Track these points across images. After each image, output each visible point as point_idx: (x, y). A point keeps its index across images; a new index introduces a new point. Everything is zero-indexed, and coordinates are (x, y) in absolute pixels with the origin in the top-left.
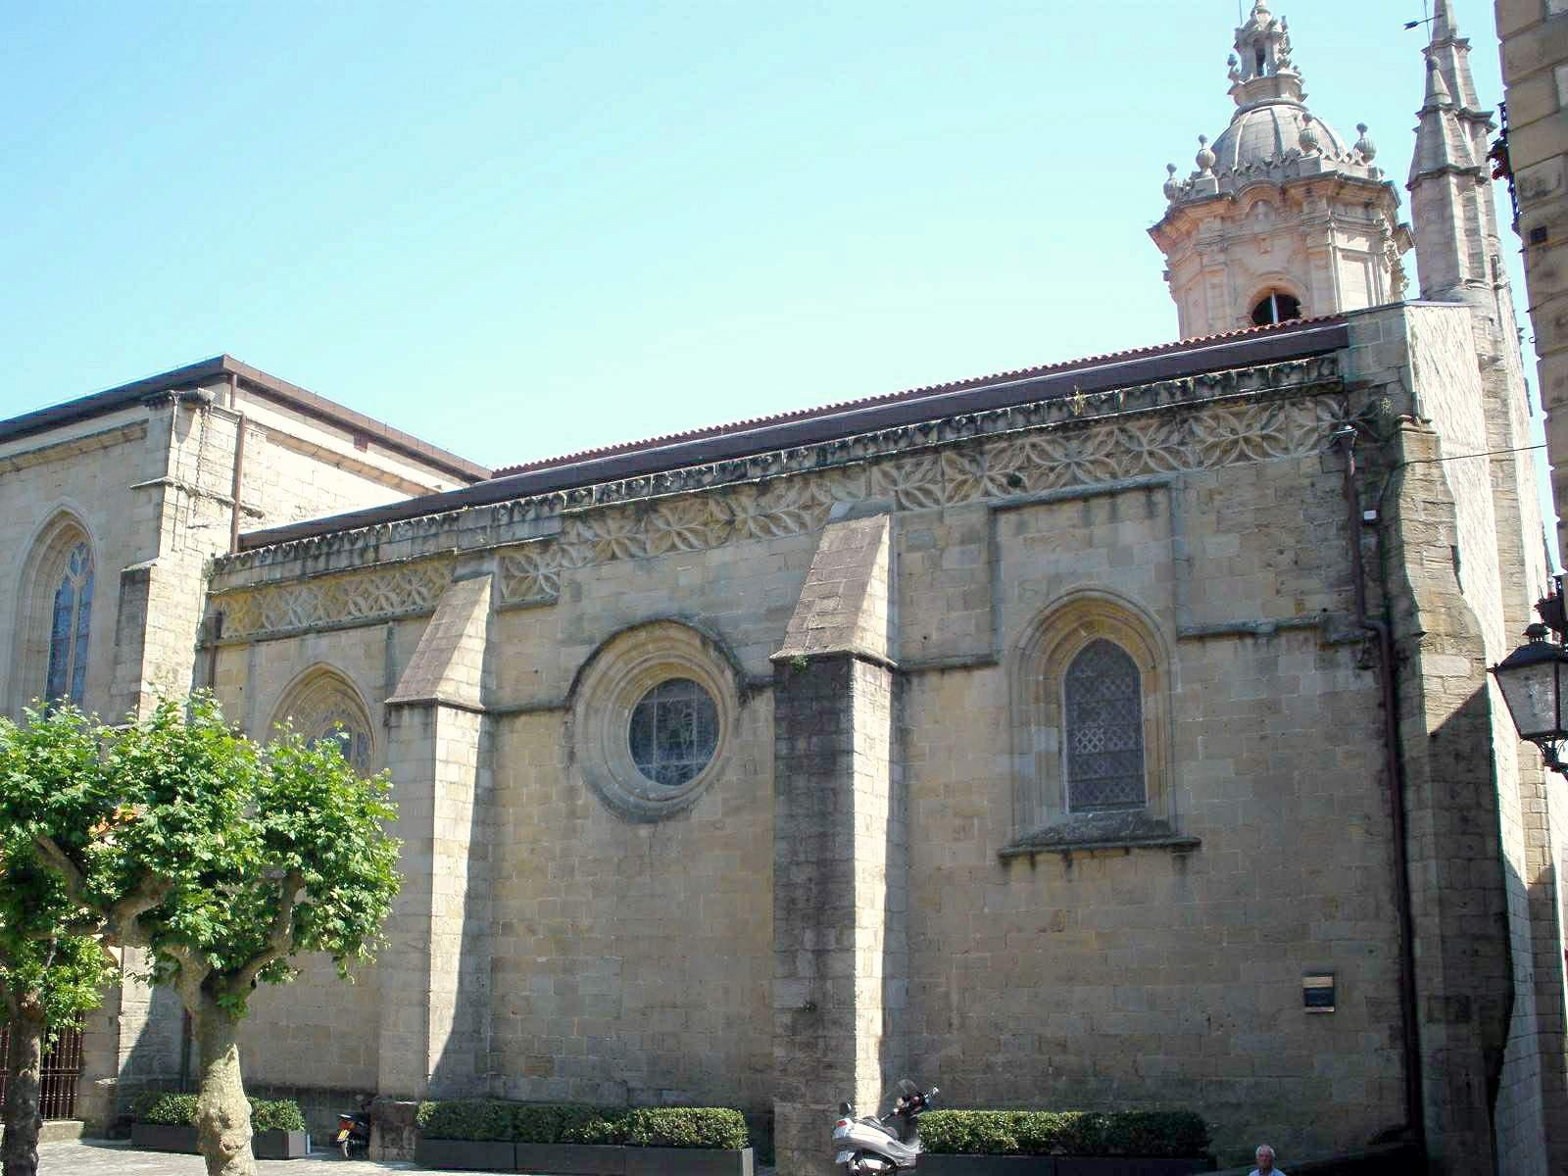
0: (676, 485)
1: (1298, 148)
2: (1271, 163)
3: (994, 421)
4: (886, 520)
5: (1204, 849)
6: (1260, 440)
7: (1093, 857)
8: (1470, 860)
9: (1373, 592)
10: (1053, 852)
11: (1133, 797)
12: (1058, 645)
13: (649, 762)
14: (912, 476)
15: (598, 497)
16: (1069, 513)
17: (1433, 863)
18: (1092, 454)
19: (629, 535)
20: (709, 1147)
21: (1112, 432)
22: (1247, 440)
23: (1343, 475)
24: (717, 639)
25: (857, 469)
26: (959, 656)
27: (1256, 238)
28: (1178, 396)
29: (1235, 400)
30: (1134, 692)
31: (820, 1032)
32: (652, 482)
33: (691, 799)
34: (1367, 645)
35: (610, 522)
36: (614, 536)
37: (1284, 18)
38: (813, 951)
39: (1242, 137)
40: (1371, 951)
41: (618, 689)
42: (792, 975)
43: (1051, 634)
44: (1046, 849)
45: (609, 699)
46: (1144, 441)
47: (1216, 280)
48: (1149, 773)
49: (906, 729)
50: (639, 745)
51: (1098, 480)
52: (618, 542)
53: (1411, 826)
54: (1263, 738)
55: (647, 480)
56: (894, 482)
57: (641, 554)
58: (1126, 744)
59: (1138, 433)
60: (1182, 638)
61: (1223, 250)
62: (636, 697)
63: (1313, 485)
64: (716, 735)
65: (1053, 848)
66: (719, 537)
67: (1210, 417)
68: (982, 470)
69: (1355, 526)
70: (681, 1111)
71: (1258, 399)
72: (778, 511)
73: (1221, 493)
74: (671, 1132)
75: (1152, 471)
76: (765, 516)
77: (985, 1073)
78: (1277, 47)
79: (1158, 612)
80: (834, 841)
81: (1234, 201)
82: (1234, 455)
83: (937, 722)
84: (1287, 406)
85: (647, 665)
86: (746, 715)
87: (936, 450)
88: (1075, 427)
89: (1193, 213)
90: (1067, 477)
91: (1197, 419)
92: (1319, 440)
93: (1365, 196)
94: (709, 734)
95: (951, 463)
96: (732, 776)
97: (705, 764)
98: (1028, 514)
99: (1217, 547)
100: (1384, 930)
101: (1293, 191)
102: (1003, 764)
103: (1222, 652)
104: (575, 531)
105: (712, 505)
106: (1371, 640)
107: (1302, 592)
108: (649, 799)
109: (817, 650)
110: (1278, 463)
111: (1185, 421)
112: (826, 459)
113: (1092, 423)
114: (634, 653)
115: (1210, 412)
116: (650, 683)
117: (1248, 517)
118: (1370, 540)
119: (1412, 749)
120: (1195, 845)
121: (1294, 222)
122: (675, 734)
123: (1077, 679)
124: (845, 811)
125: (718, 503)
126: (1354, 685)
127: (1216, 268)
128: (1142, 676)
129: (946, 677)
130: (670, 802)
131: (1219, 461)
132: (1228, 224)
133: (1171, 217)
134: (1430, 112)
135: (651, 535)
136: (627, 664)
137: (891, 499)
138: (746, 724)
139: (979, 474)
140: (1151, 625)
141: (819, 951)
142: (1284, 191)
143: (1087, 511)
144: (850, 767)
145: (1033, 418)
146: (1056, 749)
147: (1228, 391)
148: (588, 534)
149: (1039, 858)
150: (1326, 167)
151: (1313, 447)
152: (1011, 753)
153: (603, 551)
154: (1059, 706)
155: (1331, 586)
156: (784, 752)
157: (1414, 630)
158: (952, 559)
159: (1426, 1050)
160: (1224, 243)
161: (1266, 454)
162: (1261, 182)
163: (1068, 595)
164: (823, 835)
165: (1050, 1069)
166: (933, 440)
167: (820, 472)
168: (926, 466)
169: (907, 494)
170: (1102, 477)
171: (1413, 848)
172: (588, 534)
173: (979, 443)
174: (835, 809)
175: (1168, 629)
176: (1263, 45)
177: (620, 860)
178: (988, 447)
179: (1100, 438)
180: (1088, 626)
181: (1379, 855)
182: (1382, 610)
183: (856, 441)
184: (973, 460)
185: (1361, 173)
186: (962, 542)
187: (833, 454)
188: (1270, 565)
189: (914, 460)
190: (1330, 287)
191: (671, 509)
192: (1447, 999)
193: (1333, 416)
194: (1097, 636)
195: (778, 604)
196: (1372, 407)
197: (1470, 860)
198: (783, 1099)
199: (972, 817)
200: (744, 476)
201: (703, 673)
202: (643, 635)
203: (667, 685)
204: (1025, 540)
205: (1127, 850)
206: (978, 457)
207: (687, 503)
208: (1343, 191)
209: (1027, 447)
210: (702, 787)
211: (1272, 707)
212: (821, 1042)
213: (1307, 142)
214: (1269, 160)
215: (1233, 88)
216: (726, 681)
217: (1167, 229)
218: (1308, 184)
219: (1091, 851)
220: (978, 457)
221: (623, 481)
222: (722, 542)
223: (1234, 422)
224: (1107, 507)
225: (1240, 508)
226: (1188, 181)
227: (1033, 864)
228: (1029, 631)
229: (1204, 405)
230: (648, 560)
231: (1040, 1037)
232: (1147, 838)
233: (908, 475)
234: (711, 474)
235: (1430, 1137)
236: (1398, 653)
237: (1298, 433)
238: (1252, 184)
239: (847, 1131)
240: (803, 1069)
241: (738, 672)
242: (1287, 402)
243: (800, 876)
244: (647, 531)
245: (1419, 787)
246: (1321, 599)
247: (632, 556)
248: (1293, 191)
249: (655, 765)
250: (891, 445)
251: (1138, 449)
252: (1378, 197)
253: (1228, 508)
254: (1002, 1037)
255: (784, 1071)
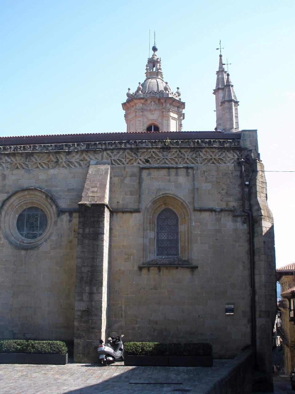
0: (40, 149)
1: (163, 90)
2: (156, 92)
3: (142, 143)
4: (109, 167)
5: (199, 269)
6: (218, 159)
7: (167, 269)
8: (271, 275)
9: (247, 204)
10: (156, 267)
11: (175, 253)
12: (157, 208)
13: (23, 231)
14: (116, 156)
15: (13, 149)
16: (164, 172)
17: (263, 276)
18: (170, 157)
19: (23, 162)
20: (55, 353)
21: (177, 151)
22: (215, 159)
23: (240, 171)
24: (51, 196)
25: (99, 152)
26: (128, 209)
27: (150, 110)
28: (196, 144)
29: (212, 148)
30: (176, 223)
31: (90, 318)
32: (32, 147)
33: (39, 244)
34: (245, 217)
35: (17, 158)
36: (18, 162)
37: (160, 58)
38: (88, 293)
39: (149, 85)
40: (244, 298)
41: (16, 208)
42: (82, 300)
43: (155, 205)
44: (153, 266)
45: (12, 211)
46: (186, 155)
47: (139, 119)
48: (181, 247)
49: (112, 228)
50: (20, 225)
51: (172, 164)
52: (19, 164)
53: (256, 265)
54: (217, 239)
55: (30, 147)
56: (111, 157)
57: (26, 168)
58: (173, 238)
59: (184, 153)
60: (195, 210)
61: (142, 112)
62: (20, 212)
63: (232, 173)
64: (46, 225)
65: (155, 266)
66: (53, 166)
67: (205, 151)
68: (138, 157)
69: (242, 185)
70: (44, 342)
71: (218, 148)
72: (73, 160)
73: (207, 172)
74: (42, 349)
75: (187, 163)
76: (68, 161)
77: (132, 330)
78: (158, 65)
79: (188, 202)
80: (97, 260)
81: (146, 100)
82: (211, 162)
83: (121, 227)
84: (226, 152)
85: (26, 202)
86: (59, 220)
87: (124, 149)
88: (166, 148)
89: (136, 101)
90: (163, 162)
91: (201, 151)
92: (233, 162)
93: (178, 105)
94: (44, 224)
95: (128, 153)
96: (54, 238)
97: (42, 234)
98: (151, 171)
99: (205, 186)
100: (247, 293)
101: (162, 100)
102: (140, 241)
103: (206, 215)
104: (5, 159)
105: (51, 156)
106: (247, 216)
107: (228, 201)
108: (24, 243)
109: (93, 202)
110: (223, 166)
111: (197, 151)
112: (89, 147)
113: (172, 148)
114: (22, 198)
115: (205, 150)
116: (25, 207)
117: (214, 179)
118: (247, 190)
119: (257, 245)
120: (197, 267)
121: (161, 108)
122: (32, 223)
123: (160, 218)
124: (100, 251)
125: (53, 156)
126: (241, 227)
127: (140, 116)
128: (179, 220)
129: (124, 214)
130: (31, 244)
131: (206, 163)
132: (144, 105)
133: (128, 101)
134: (228, 86)
135: (30, 163)
136: (19, 201)
137: (110, 160)
138: (59, 223)
139: (137, 158)
140: (186, 206)
141: (91, 293)
142: (159, 100)
143: (169, 172)
144: (103, 238)
145: (154, 144)
146: (154, 238)
147: (210, 145)
148: (9, 160)
149: (151, 268)
150: (170, 96)
151: (232, 163)
152: (144, 238)
153: (14, 166)
154: (155, 225)
155: (236, 200)
156: (81, 232)
157: (260, 215)
158: (127, 181)
159: (258, 324)
160: (143, 110)
161: (220, 163)
162: (154, 97)
163: (162, 195)
164: (93, 258)
165: (152, 329)
166: (123, 146)
167: (87, 151)
168: (121, 153)
169: (114, 160)
170: (173, 163)
171: (256, 271)
172: (9, 160)
173: (138, 149)
174: (97, 250)
175: (191, 207)
176: (155, 64)
177: (14, 261)
178: (140, 150)
179: (172, 153)
180: (165, 204)
181: (247, 273)
182: (249, 208)
183: (99, 143)
184: (135, 154)
185: (177, 99)
186: (131, 176)
187: (91, 146)
188: (219, 193)
189: (117, 151)
190: (168, 125)
191: (37, 156)
192: (266, 311)
193: (238, 156)
194: (167, 207)
195: (71, 188)
196: (248, 155)
197: (271, 275)
198: (77, 338)
199: (131, 255)
200: (62, 149)
201: (44, 206)
202: (26, 192)
203: (30, 209)
204: (150, 178)
205: (177, 268)
206: (137, 153)
207: (43, 155)
208: (174, 103)
209: (152, 152)
210: (43, 240)
211: (219, 231)
212: (90, 321)
213: (166, 89)
214: (155, 91)
215: (146, 72)
216: (53, 209)
217: (127, 104)
218: (166, 99)
219: (167, 267)
220: (137, 153)
221: (22, 146)
222: (54, 168)
223: (211, 153)
224: (175, 171)
225: (212, 177)
226: (134, 93)
227: (149, 270)
228: (150, 204)
229: (204, 148)
230: (29, 170)
231: (149, 320)
232: (183, 265)
233: (115, 155)
234: (51, 147)
235: (258, 348)
236: (254, 220)
237: (228, 159)
238: (151, 97)
239: (103, 349)
240: (84, 329)
241: (57, 206)
242: (226, 150)
243: (85, 270)
244: (29, 161)
245: (259, 256)
246: (233, 204)
247: (24, 168)
248: (162, 100)
249: (25, 232)
250: (110, 146)
251: (184, 157)
252: (181, 106)
253: (209, 176)
254: (138, 320)
255: (78, 329)
